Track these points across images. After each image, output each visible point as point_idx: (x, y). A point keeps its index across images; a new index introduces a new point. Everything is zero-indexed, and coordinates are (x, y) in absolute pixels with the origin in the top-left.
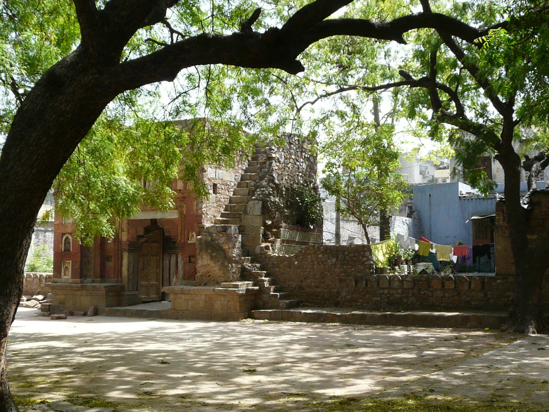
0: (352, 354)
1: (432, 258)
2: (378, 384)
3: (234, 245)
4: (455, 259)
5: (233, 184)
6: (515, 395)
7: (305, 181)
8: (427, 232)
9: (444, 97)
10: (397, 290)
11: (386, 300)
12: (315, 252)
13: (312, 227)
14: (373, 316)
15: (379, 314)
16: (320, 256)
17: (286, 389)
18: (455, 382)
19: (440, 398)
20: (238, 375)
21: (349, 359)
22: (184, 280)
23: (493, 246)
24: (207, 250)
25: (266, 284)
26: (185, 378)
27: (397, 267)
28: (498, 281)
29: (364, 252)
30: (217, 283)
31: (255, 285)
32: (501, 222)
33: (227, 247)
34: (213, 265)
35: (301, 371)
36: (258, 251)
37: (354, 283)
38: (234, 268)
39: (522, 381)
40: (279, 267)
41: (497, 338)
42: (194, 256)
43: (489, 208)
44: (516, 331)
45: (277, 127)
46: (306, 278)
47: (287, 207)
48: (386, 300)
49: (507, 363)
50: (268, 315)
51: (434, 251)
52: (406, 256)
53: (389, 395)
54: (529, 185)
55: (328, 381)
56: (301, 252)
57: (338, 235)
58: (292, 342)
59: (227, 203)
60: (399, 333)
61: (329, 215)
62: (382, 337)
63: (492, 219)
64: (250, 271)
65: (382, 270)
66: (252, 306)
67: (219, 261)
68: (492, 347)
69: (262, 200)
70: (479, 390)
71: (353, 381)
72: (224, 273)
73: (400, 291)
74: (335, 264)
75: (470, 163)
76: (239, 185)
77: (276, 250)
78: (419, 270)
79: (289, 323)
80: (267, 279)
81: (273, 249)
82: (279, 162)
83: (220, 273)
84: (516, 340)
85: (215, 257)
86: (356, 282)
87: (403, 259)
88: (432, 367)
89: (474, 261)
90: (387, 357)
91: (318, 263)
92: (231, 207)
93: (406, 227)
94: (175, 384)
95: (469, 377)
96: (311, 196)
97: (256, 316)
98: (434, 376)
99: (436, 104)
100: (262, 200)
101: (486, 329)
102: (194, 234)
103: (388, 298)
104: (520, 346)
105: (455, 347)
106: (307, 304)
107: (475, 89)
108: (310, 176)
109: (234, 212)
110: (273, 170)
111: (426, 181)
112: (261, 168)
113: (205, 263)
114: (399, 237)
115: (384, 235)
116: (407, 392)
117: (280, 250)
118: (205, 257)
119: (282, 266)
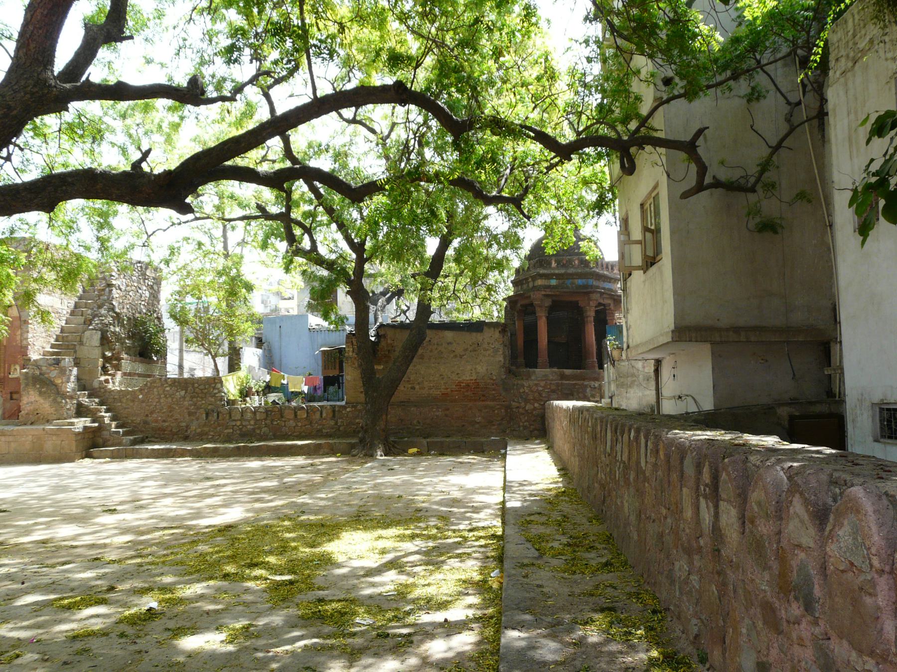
0: (213, 486)
1: (283, 389)
2: (248, 511)
3: (69, 379)
4: (305, 389)
5: (65, 312)
6: (376, 509)
7: (148, 310)
8: (277, 363)
9: (298, 231)
10: (249, 421)
11: (238, 432)
12: (162, 385)
13: (155, 359)
14: (226, 448)
15: (232, 446)
16: (168, 389)
17: (157, 523)
18: (322, 503)
19: (312, 518)
20: (97, 516)
21: (211, 491)
22: (4, 419)
23: (342, 376)
24: (34, 385)
25: (107, 421)
26: (36, 524)
27: (248, 399)
28: (348, 410)
29: (215, 381)
30: (48, 421)
31: (93, 422)
32: (351, 354)
33: (60, 381)
34: (42, 401)
35: (166, 506)
36: (96, 384)
37: (204, 415)
38: (71, 405)
39: (380, 497)
40: (121, 402)
41: (349, 462)
42: (17, 392)
43: (339, 340)
44: (365, 455)
45: (125, 253)
46: (152, 413)
47: (129, 338)
48: (238, 432)
49: (364, 483)
50: (109, 454)
51: (285, 382)
52: (257, 387)
53: (263, 519)
54: (376, 320)
55: (197, 513)
56: (146, 385)
57: (181, 367)
58: (144, 479)
59: (58, 333)
60: (254, 464)
61: (173, 345)
62: (239, 469)
63: (340, 351)
64: (87, 407)
65: (231, 403)
66: (91, 444)
67: (49, 397)
68: (347, 471)
69: (101, 330)
70: (346, 509)
71: (222, 510)
72: (56, 410)
73: (252, 422)
74: (184, 397)
75: (322, 300)
76: (72, 313)
77: (116, 383)
78: (270, 400)
79: (135, 461)
80: (107, 415)
81: (114, 383)
82: (120, 289)
83: (52, 410)
84: (366, 463)
85: (45, 393)
86: (207, 415)
87: (254, 390)
88: (296, 492)
89: (325, 391)
90: (250, 486)
91: (165, 396)
92: (63, 337)
93: (257, 359)
94: (27, 531)
95: (333, 498)
96: (155, 325)
97: (95, 455)
98: (301, 500)
99: (291, 239)
100: (101, 330)
101: (411, 451)
102: (18, 367)
103: (240, 429)
104: (372, 468)
105: (312, 472)
106: (153, 439)
107: (327, 225)
108: (153, 305)
109: (67, 343)
110: (113, 298)
111: (268, 311)
112: (99, 296)
113: (31, 399)
114: (250, 369)
115: (234, 366)
116: (281, 516)
117: (121, 383)
118: (32, 392)
119: (124, 400)
